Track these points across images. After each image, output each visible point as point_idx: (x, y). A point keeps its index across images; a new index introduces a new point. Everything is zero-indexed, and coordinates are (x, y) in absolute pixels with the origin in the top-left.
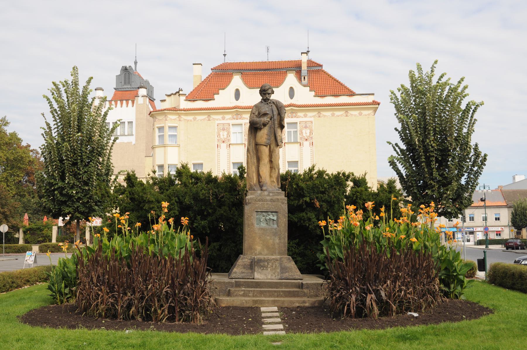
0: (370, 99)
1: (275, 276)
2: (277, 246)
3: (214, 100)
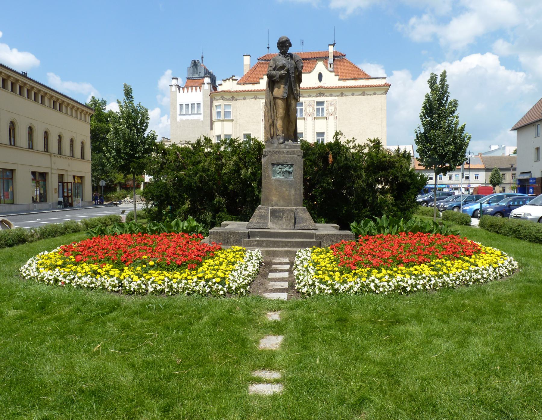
0: (382, 82)
1: (290, 227)
2: (292, 197)
3: (259, 83)
